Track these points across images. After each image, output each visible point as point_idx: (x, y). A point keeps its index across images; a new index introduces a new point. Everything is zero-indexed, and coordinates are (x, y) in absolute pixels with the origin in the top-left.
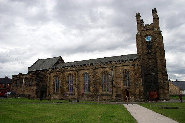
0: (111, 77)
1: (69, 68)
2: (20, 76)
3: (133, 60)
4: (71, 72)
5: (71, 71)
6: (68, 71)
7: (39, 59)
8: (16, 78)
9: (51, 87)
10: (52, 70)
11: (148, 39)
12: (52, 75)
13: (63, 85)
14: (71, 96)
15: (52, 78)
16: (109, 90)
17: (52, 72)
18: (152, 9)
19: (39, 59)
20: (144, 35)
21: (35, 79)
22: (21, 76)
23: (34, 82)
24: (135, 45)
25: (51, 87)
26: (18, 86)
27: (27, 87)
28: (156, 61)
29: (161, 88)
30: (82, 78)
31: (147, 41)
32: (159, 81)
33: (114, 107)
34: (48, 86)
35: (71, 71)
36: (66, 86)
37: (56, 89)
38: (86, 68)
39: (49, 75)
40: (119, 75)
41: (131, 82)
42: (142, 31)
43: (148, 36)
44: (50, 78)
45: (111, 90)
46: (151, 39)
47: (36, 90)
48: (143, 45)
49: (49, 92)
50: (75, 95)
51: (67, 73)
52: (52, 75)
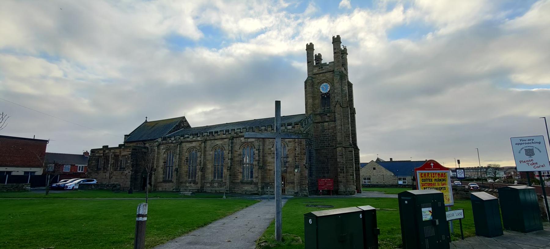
0: (257, 152)
1: (191, 137)
2: (104, 151)
3: (293, 124)
4: (194, 144)
5: (195, 141)
6: (190, 142)
7: (146, 120)
8: (97, 155)
9: (160, 170)
10: (163, 140)
11: (325, 88)
12: (163, 149)
13: (180, 166)
14: (192, 184)
15: (162, 154)
16: (254, 175)
17: (163, 144)
18: (333, 37)
19: (146, 120)
20: (319, 81)
21: (131, 156)
22: (107, 151)
23: (129, 161)
24: (446, 214)
25: (160, 170)
26: (100, 169)
27: (116, 170)
28: (335, 127)
29: (341, 173)
30: (211, 154)
31: (323, 92)
32: (338, 160)
33: (89, 232)
34: (155, 167)
35: (194, 143)
36: (185, 168)
37: (169, 172)
38: (218, 137)
39: (156, 150)
40: (270, 149)
41: (289, 162)
42: (314, 74)
43: (325, 84)
44: (159, 153)
45: (257, 174)
46: (328, 90)
47: (131, 175)
48: (314, 98)
49: (156, 180)
50: (198, 184)
51: (189, 145)
52: (163, 149)
